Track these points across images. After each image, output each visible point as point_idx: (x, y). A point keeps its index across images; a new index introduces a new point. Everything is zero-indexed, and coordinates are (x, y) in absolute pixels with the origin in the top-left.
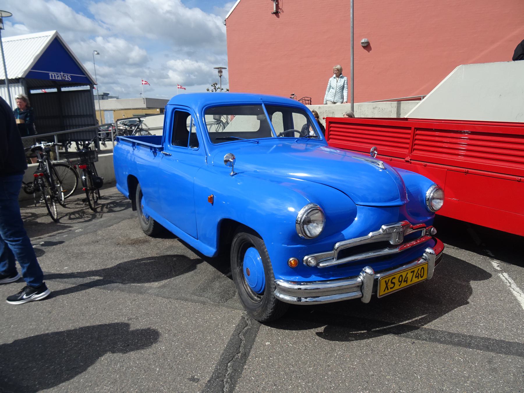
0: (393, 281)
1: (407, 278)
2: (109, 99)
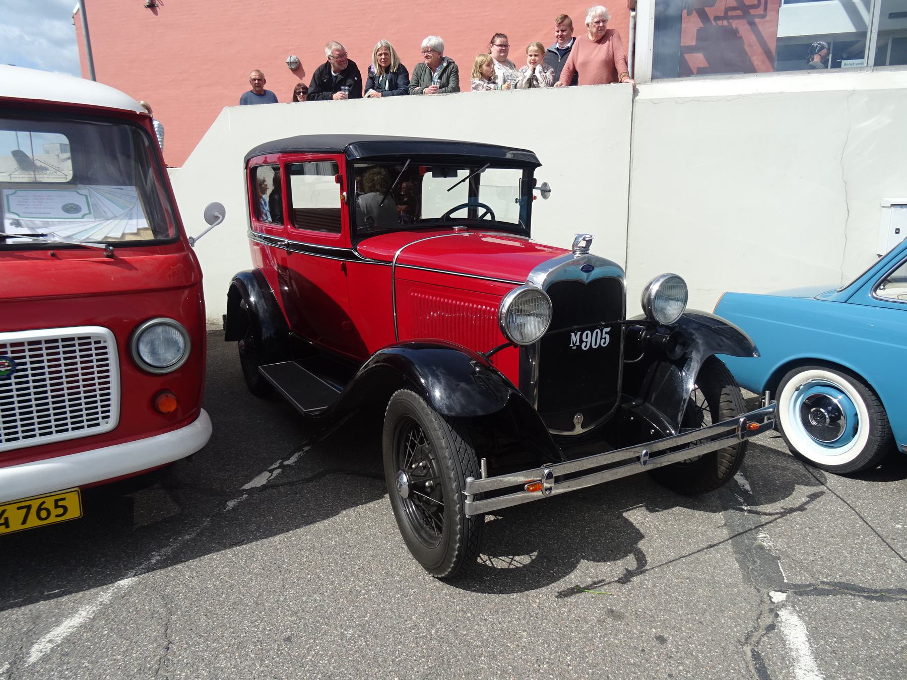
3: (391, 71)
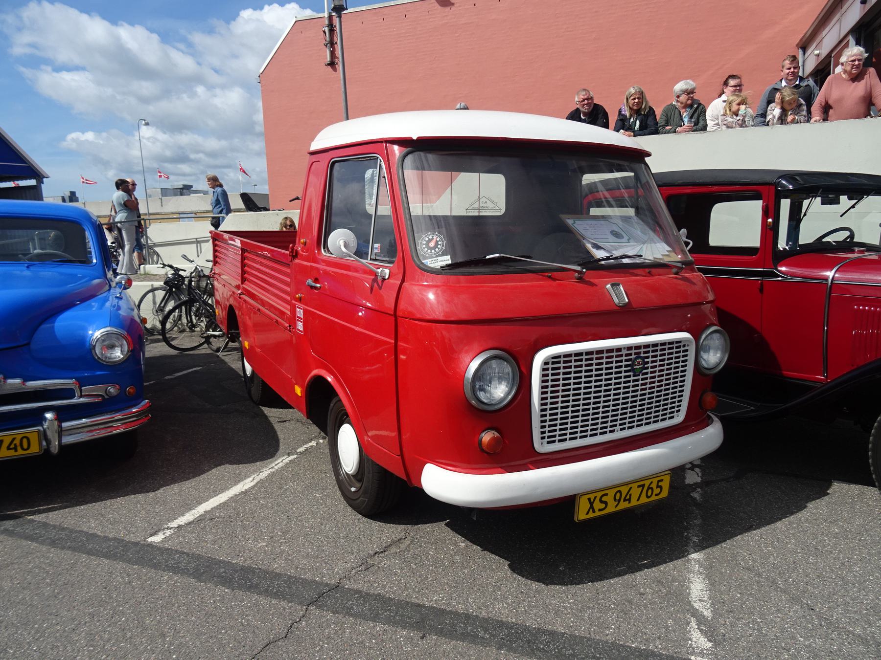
0: (604, 499)
1: (630, 495)
2: (191, 195)
3: (643, 113)
